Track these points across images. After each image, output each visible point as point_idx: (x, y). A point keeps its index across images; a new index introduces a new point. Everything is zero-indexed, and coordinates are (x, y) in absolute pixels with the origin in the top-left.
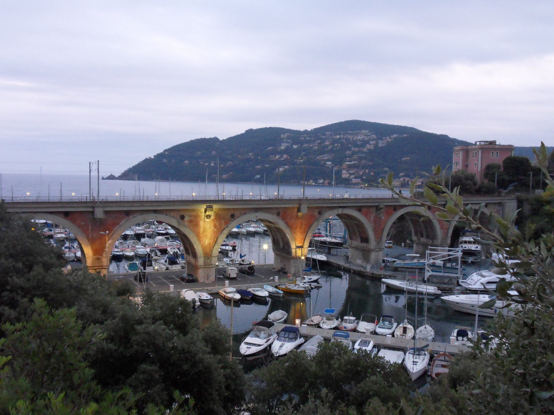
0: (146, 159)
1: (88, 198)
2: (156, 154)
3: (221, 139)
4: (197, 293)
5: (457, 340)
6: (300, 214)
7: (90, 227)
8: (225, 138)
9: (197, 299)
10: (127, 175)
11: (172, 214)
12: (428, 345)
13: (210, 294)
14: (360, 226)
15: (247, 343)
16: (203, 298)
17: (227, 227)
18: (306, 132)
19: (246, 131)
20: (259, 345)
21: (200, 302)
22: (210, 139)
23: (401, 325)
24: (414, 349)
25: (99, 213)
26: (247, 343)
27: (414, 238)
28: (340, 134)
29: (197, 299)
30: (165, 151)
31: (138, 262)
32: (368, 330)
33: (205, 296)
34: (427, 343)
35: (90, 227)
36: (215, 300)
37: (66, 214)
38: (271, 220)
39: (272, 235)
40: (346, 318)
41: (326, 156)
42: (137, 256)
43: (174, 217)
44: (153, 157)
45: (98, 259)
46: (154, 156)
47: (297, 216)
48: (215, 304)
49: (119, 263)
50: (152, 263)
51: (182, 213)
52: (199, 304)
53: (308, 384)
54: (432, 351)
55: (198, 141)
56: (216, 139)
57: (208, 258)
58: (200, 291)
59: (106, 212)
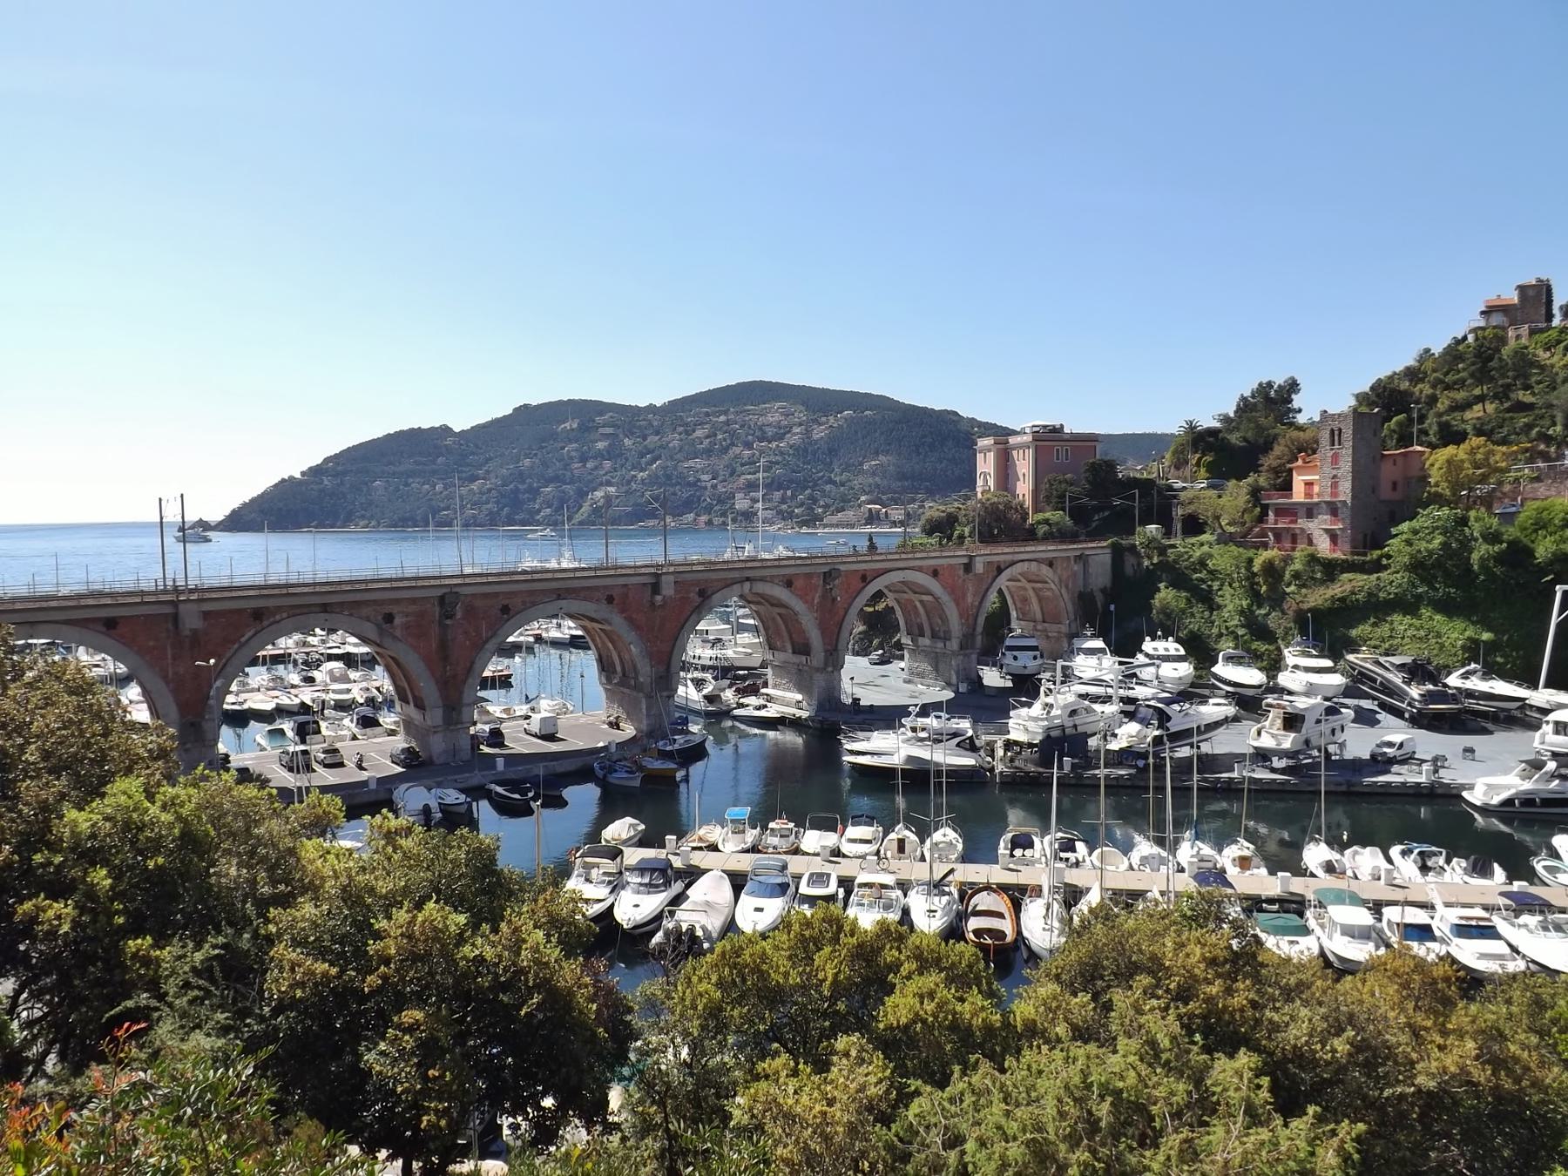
0: (283, 481)
1: (160, 583)
2: (305, 468)
3: (457, 430)
4: (433, 791)
5: (1012, 856)
6: (659, 598)
7: (169, 652)
8: (467, 427)
9: (434, 805)
10: (241, 521)
11: (365, 611)
12: (952, 871)
13: (462, 791)
14: (790, 619)
15: (1010, 648)
16: (448, 801)
17: (494, 635)
18: (651, 408)
19: (516, 410)
20: (600, 901)
21: (441, 811)
22: (432, 429)
23: (893, 836)
24: (928, 884)
25: (191, 621)
26: (1010, 648)
27: (906, 640)
28: (726, 413)
29: (434, 805)
30: (327, 460)
31: (287, 726)
32: (824, 847)
33: (453, 796)
34: (950, 866)
35: (169, 652)
36: (475, 804)
37: (110, 624)
38: (594, 615)
39: (596, 646)
40: (772, 825)
41: (698, 463)
42: (281, 712)
43: (368, 619)
44: (298, 476)
45: (192, 724)
46: (303, 474)
47: (653, 604)
48: (476, 815)
49: (239, 731)
50: (319, 727)
51: (387, 609)
52: (440, 815)
53: (681, 690)
54: (963, 884)
55: (400, 435)
56: (445, 430)
57: (454, 709)
58: (439, 785)
59: (206, 615)
